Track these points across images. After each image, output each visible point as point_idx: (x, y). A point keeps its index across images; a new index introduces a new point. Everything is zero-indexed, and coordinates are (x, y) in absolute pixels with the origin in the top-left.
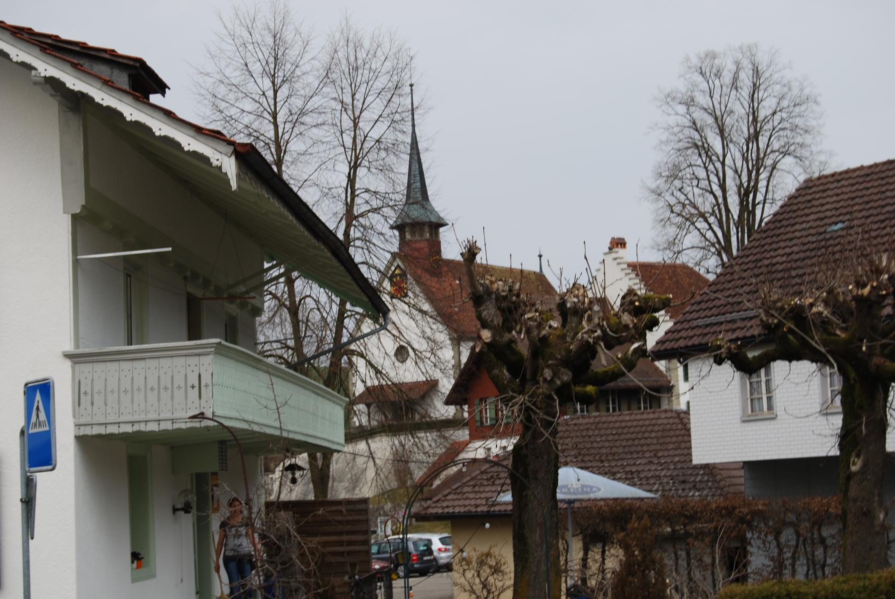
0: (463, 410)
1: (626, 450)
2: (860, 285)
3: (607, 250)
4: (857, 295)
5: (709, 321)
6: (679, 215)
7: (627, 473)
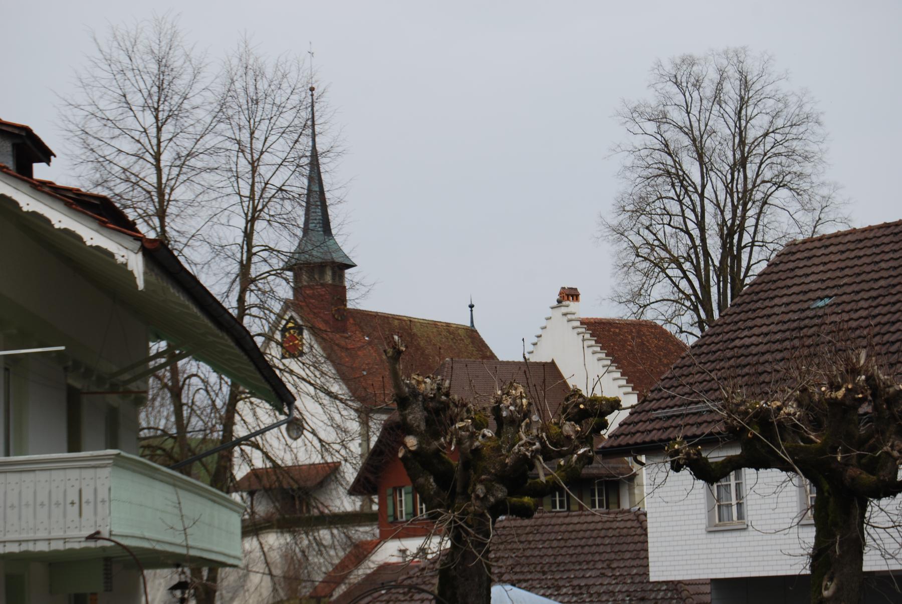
0: (372, 501)
1: (574, 559)
4: (831, 398)
5: (670, 412)
6: (646, 259)
7: (574, 588)
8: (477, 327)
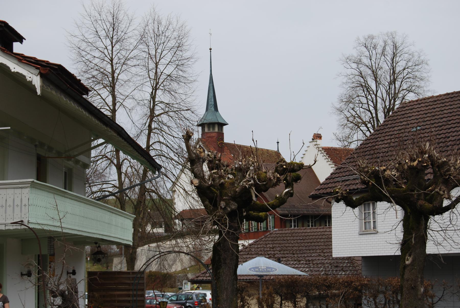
1: (307, 248)
2: (413, 160)
3: (311, 140)
4: (411, 166)
6: (352, 122)
7: (306, 261)
8: (280, 151)
